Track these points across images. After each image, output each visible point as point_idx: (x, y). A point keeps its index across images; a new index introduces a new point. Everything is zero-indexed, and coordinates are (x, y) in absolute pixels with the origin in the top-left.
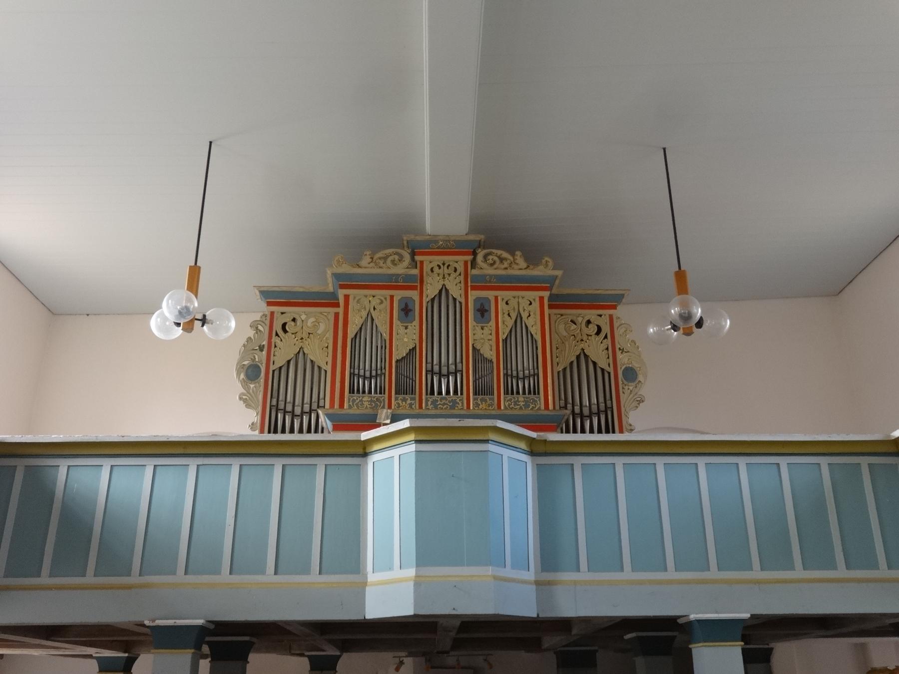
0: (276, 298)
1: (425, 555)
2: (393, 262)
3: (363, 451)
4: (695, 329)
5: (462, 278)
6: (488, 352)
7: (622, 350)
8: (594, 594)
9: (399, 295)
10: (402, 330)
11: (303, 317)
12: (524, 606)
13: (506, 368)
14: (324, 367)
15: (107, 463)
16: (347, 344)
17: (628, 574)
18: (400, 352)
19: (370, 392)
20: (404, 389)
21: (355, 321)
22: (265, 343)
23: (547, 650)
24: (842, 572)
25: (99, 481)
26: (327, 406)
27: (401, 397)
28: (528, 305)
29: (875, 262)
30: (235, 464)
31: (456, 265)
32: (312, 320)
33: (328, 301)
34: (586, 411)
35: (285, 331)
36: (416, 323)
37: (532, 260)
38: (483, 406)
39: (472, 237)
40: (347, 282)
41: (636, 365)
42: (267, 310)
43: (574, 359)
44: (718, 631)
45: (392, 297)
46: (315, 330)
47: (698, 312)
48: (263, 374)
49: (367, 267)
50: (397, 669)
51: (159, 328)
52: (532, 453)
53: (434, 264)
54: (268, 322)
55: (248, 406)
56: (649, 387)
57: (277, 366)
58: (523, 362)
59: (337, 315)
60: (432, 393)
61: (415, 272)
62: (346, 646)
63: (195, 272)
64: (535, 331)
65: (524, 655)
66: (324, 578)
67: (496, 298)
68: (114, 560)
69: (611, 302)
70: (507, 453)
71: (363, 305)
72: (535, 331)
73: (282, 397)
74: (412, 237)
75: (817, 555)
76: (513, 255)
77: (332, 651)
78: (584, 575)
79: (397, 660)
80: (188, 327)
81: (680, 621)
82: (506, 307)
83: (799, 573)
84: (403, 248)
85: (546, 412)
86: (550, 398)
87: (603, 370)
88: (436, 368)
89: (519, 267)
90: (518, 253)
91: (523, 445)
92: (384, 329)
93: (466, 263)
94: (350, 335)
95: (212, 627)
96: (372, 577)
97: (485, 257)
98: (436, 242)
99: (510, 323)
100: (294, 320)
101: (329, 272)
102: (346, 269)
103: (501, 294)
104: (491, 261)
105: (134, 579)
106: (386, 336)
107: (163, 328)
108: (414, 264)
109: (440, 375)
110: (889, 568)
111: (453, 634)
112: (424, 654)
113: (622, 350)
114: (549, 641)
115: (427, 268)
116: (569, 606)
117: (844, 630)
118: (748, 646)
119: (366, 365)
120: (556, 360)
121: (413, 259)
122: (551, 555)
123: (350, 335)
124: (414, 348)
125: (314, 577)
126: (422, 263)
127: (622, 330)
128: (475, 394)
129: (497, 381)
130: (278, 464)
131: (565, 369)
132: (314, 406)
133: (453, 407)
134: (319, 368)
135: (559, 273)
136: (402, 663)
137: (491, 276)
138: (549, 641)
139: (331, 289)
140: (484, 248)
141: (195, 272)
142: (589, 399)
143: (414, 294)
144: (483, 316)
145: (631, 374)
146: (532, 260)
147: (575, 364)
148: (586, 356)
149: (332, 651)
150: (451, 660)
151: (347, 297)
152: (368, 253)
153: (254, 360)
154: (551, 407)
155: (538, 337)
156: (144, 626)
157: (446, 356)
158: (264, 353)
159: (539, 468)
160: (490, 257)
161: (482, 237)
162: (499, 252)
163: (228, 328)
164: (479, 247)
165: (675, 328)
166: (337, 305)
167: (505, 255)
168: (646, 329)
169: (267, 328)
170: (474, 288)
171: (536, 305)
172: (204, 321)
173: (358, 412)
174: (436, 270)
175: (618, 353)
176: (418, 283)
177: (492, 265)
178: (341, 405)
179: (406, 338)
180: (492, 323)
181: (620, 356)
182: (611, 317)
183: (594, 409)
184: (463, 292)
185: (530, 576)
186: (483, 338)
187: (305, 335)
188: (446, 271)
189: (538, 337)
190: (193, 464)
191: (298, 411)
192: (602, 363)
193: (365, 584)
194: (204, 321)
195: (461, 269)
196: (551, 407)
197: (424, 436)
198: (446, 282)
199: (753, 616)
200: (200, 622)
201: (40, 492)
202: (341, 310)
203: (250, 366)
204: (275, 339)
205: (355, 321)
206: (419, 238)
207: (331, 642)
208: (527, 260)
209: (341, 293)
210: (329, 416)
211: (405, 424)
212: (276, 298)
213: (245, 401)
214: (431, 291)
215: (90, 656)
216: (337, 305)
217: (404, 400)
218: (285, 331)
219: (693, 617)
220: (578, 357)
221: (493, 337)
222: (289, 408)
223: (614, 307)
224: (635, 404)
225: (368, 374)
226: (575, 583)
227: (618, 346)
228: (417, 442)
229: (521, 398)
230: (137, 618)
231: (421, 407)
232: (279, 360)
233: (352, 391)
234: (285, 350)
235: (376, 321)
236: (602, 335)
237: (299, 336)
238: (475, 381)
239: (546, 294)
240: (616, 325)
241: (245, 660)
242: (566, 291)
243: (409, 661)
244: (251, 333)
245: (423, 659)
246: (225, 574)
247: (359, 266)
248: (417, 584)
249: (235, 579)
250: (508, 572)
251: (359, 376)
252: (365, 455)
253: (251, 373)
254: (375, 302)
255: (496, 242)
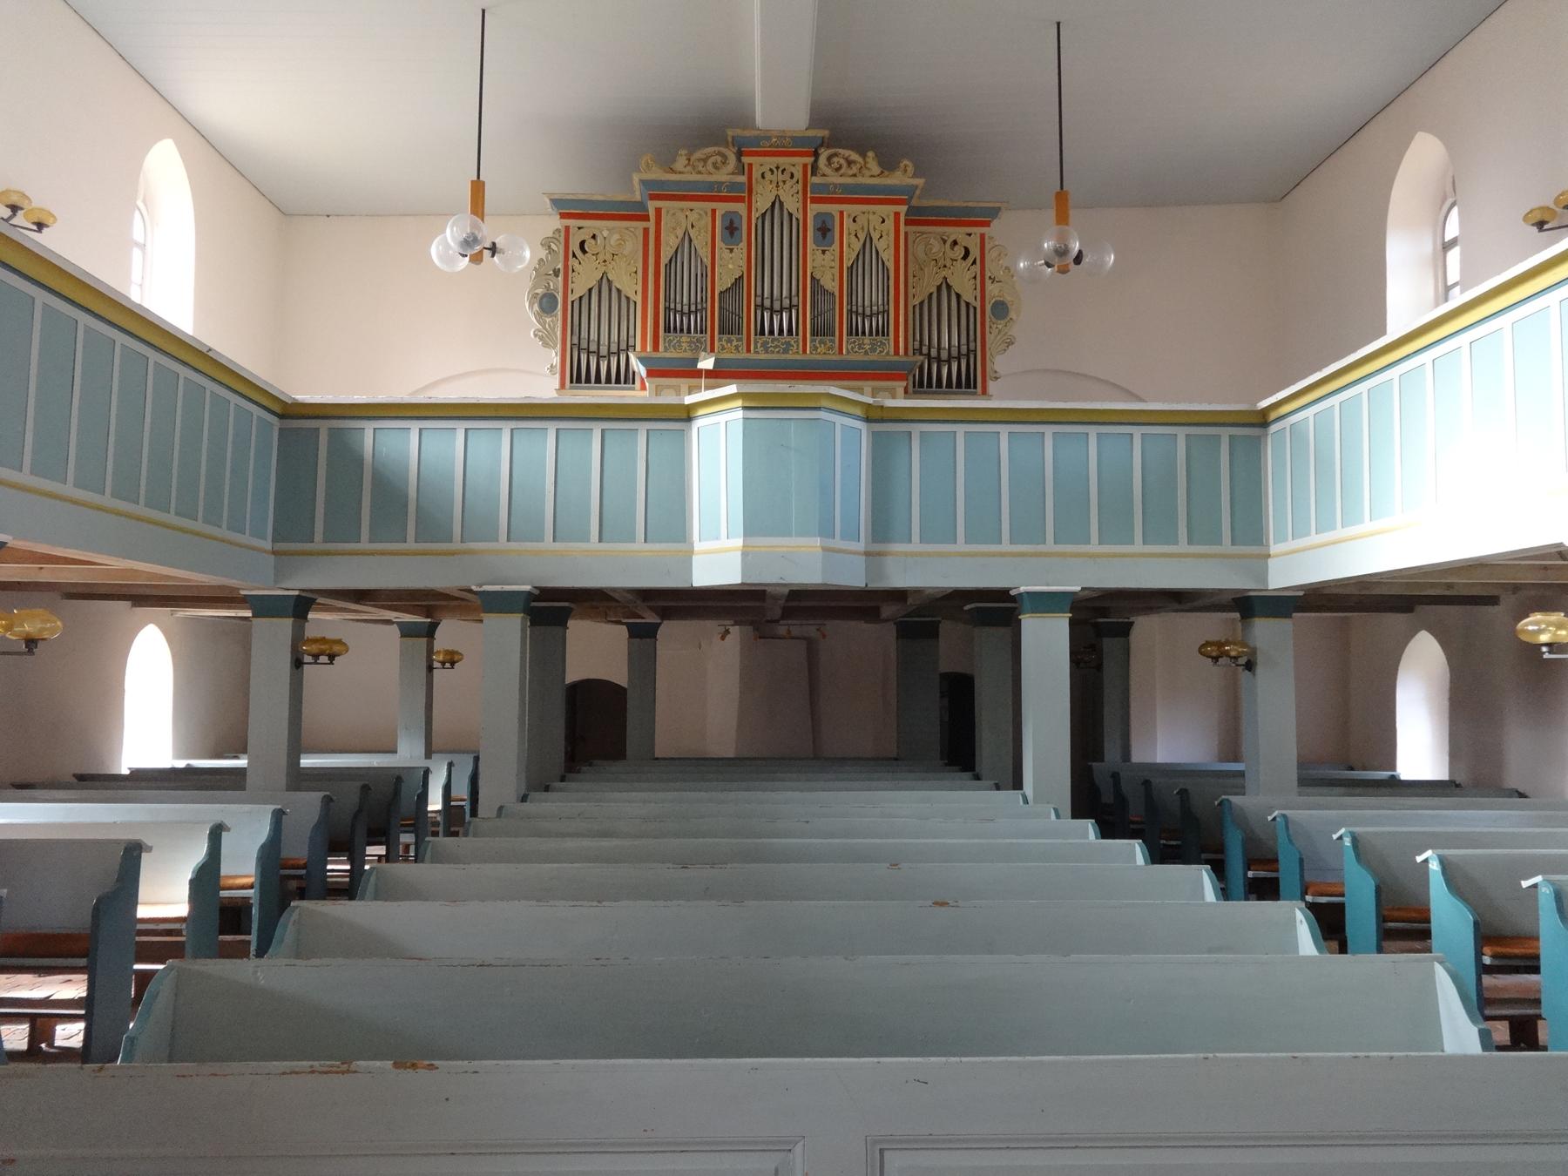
0: (570, 209)
1: (754, 525)
2: (715, 165)
3: (686, 415)
4: (1072, 266)
5: (800, 186)
6: (830, 284)
7: (993, 280)
8: (926, 566)
9: (722, 208)
10: (726, 254)
11: (605, 233)
12: (853, 576)
13: (850, 303)
14: (633, 297)
15: (415, 426)
16: (662, 272)
17: (961, 546)
18: (724, 282)
19: (689, 331)
20: (729, 328)
21: (670, 243)
22: (560, 266)
23: (887, 620)
24: (1183, 547)
25: (409, 447)
26: (638, 348)
27: (725, 337)
28: (878, 223)
29: (1345, 148)
30: (552, 427)
31: (793, 170)
32: (616, 236)
33: (631, 213)
34: (944, 355)
35: (584, 251)
36: (744, 244)
37: (888, 164)
38: (821, 349)
39: (811, 133)
40: (660, 192)
41: (1008, 298)
42: (556, 223)
43: (934, 290)
44: (1046, 602)
45: (714, 211)
46: (620, 255)
47: (1076, 247)
48: (560, 306)
49: (684, 172)
50: (723, 638)
51: (440, 257)
52: (868, 420)
53: (766, 169)
54: (562, 239)
55: (545, 345)
56: (1023, 323)
57: (576, 296)
58: (871, 295)
59: (646, 231)
60: (762, 333)
61: (743, 179)
62: (666, 614)
63: (478, 188)
64: (888, 256)
65: (863, 625)
66: (648, 546)
67: (842, 213)
68: (433, 527)
69: (980, 218)
70: (840, 420)
71: (678, 219)
72: (888, 256)
73: (584, 334)
74: (738, 132)
75: (1159, 528)
76: (864, 155)
77: (651, 618)
78: (916, 546)
79: (722, 629)
80: (477, 259)
81: (1012, 593)
82: (853, 227)
83: (1138, 547)
84: (727, 146)
85: (896, 358)
86: (901, 339)
87: (968, 304)
88: (767, 303)
89: (870, 173)
90: (871, 154)
91: (858, 411)
92: (705, 253)
93: (805, 166)
94: (664, 260)
95: (537, 592)
96: (698, 546)
97: (829, 159)
98: (769, 138)
99: (857, 246)
100: (594, 237)
101: (636, 178)
102: (657, 174)
103: (847, 208)
104: (836, 165)
105: (456, 545)
106: (707, 261)
107: (446, 258)
108: (740, 168)
109: (772, 310)
110: (1233, 544)
111: (782, 602)
112: (752, 623)
113: (993, 280)
114: (888, 610)
115: (756, 174)
116: (899, 578)
117: (1196, 604)
118: (200, 515)
119: (684, 298)
120: (911, 291)
121: (739, 160)
122: (883, 526)
123: (664, 260)
124: (741, 277)
125: (639, 545)
126: (750, 165)
127: (994, 254)
128: (813, 334)
129: (840, 321)
130: (597, 428)
131: (921, 303)
132: (623, 346)
133: (786, 351)
134: (628, 299)
135: (920, 182)
136: (727, 632)
137: (835, 186)
138: (888, 610)
139: (638, 197)
140: (828, 147)
141: (478, 188)
142: (948, 338)
143: (741, 208)
144: (824, 236)
145: (1001, 309)
146: (888, 164)
147: (935, 296)
148: (949, 287)
149: (651, 618)
150: (782, 630)
151: (658, 211)
152: (684, 152)
153: (548, 288)
154: (901, 351)
155: (891, 265)
156: (470, 591)
157: (778, 286)
158: (560, 278)
159: (875, 436)
160: (835, 159)
161: (826, 133)
162: (847, 153)
163: (522, 259)
164: (822, 145)
165: (1048, 265)
166: (646, 218)
167: (854, 156)
168: (1022, 253)
169: (562, 247)
170: (814, 200)
171: (890, 223)
172: (493, 249)
173: (675, 355)
174: (768, 175)
175: (988, 282)
176: (744, 194)
177: (837, 170)
178: (656, 347)
179: (731, 265)
180: (836, 246)
181: (989, 287)
182: (982, 236)
183: (954, 352)
184: (800, 205)
185: (860, 546)
186: (824, 265)
187: (608, 257)
188: (781, 177)
189: (891, 265)
190: (506, 427)
191: (604, 351)
192: (967, 296)
193: (691, 552)
194: (493, 249)
195: (798, 175)
196: (901, 351)
197: (753, 403)
198: (781, 192)
199: (1083, 589)
200: (527, 588)
201: (348, 460)
202: (651, 225)
203: (545, 295)
204: (571, 260)
205: (670, 243)
206: (747, 133)
207: (651, 608)
208: (880, 164)
209: (652, 206)
210: (641, 360)
211: (731, 389)
212: (570, 209)
213: (541, 338)
214: (762, 203)
215: (388, 622)
216: (646, 218)
217: (730, 341)
218: (584, 251)
219: (1023, 589)
220: (939, 288)
221: (836, 264)
222: (593, 347)
223: (987, 224)
224: (1003, 346)
225: (686, 309)
226: (906, 554)
227: (988, 274)
228: (745, 408)
229: (867, 340)
230: (464, 584)
231: (748, 350)
232: (579, 289)
233: (668, 330)
234: (585, 276)
235: (695, 242)
236: (970, 259)
237: (601, 258)
238: (813, 319)
239: (903, 209)
240: (987, 247)
241: (564, 625)
242: (925, 203)
243: (735, 631)
244: (543, 253)
245: (750, 628)
246: (548, 543)
247: (673, 171)
248: (745, 554)
249: (559, 546)
250: (838, 543)
251: (676, 312)
252: (689, 419)
253: (546, 304)
254: (693, 217)
255: (846, 134)
